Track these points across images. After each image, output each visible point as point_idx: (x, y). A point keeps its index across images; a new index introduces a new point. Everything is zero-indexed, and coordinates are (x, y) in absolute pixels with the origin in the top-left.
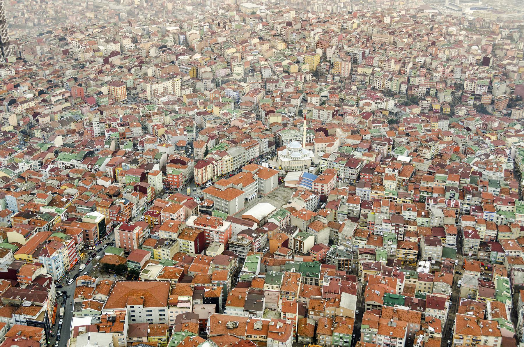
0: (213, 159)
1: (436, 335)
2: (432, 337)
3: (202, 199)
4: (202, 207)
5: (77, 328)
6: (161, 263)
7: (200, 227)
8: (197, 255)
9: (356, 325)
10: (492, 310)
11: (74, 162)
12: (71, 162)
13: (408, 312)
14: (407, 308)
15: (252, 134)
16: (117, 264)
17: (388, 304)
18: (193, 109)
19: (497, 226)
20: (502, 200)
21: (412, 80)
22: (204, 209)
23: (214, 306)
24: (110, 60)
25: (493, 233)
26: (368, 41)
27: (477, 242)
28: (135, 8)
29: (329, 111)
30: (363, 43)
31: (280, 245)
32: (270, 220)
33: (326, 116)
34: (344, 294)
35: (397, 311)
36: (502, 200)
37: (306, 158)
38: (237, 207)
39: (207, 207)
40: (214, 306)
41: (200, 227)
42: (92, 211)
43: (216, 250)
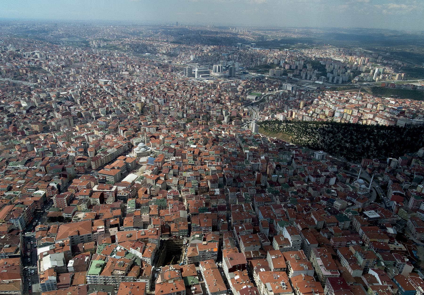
0: (100, 156)
1: (225, 222)
2: (224, 224)
3: (98, 176)
4: (100, 180)
5: (41, 254)
6: (83, 212)
7: (101, 190)
8: (101, 205)
9: (72, 257)
10: (245, 207)
11: (19, 166)
12: (18, 166)
13: (211, 214)
14: (210, 213)
15: (118, 142)
16: (57, 216)
17: (201, 212)
18: (83, 133)
19: (239, 171)
20: (239, 160)
21: (188, 111)
22: (101, 181)
23: (117, 228)
24: (30, 111)
25: (237, 174)
26: (165, 95)
27: (232, 179)
28: (39, 84)
29: (285, 49)
30: (163, 96)
31: (144, 193)
32: (136, 182)
33: (152, 130)
34: (181, 211)
35: (206, 215)
36: (239, 160)
37: (148, 151)
38: (118, 178)
39: (102, 180)
40: (117, 228)
41: (101, 190)
42: (36, 190)
43: (110, 201)
